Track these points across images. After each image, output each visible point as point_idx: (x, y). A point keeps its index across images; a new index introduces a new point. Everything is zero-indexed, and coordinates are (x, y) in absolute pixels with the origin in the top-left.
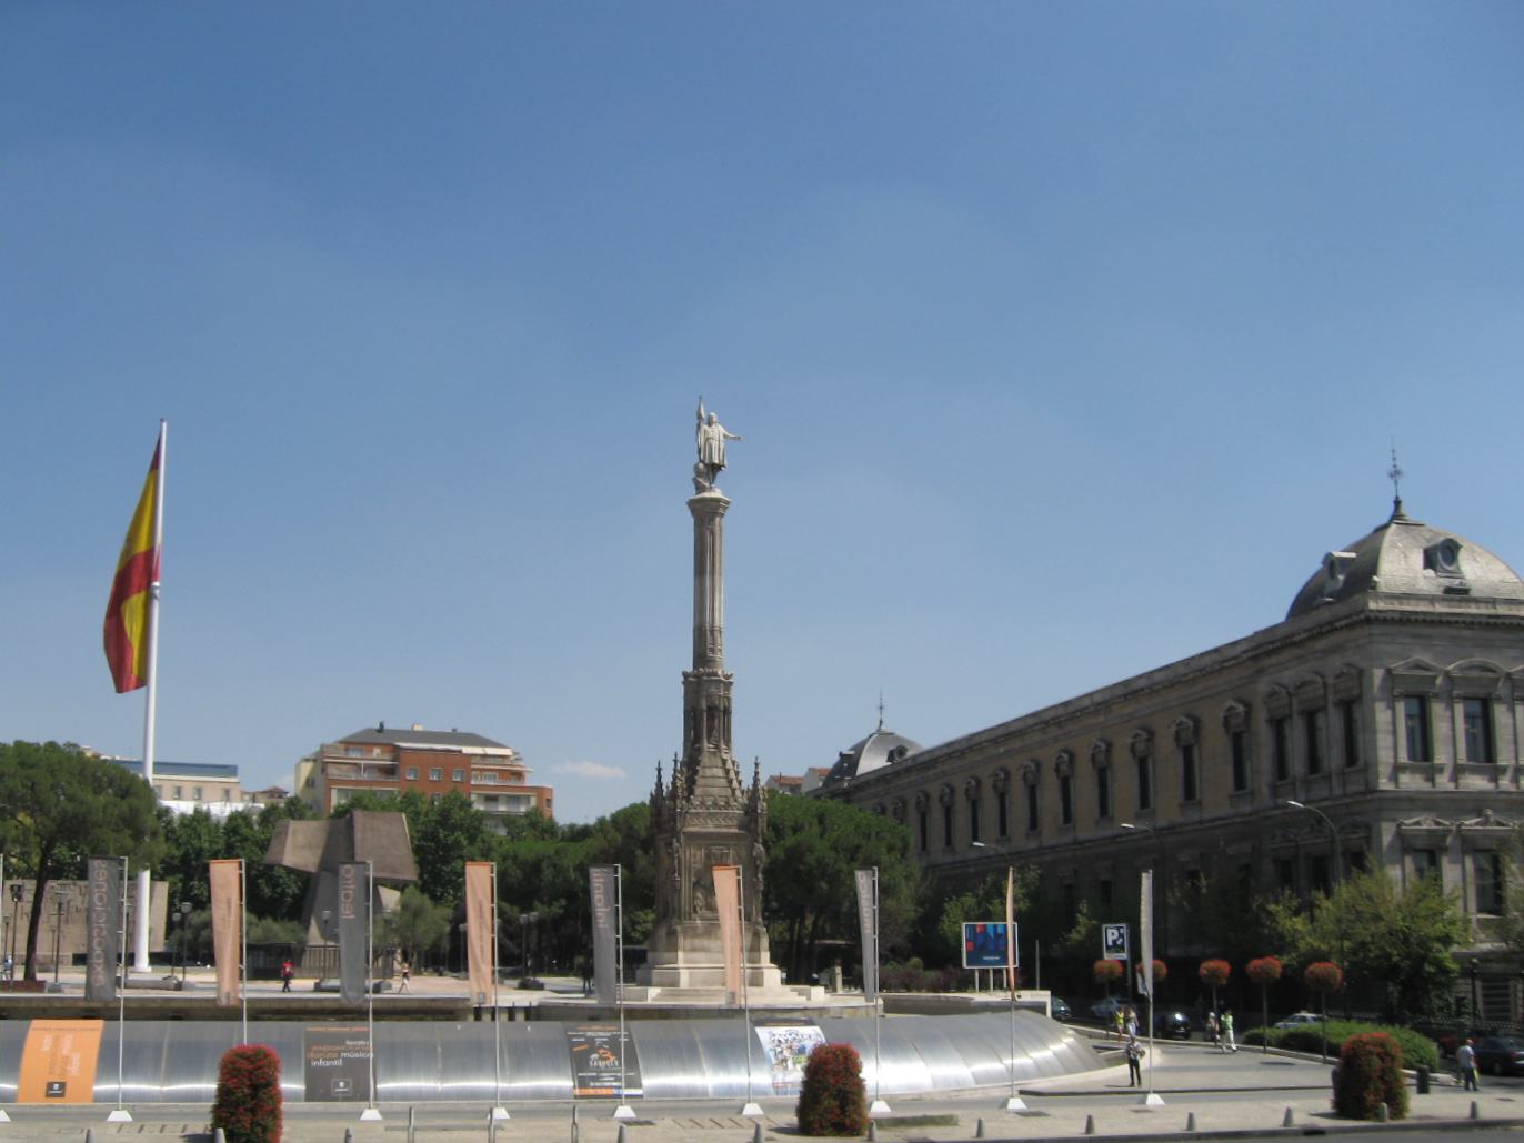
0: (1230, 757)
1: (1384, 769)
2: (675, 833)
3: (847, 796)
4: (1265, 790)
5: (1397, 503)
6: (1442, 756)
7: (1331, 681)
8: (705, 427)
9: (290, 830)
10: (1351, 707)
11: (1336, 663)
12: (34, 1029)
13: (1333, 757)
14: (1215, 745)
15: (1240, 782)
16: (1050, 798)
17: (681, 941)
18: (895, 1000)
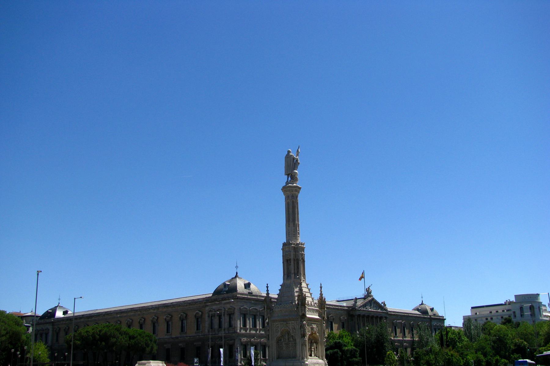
0: (196, 323)
1: (239, 328)
4: (206, 331)
5: (237, 273)
7: (227, 309)
10: (231, 315)
13: (225, 325)
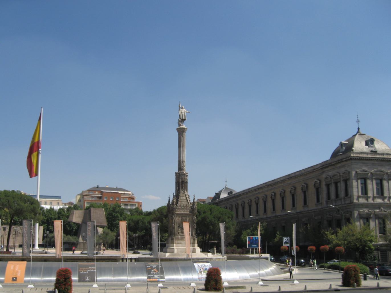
0: (316, 194)
1: (355, 197)
2: (173, 214)
3: (217, 204)
4: (325, 203)
5: (359, 129)
6: (370, 194)
7: (341, 174)
8: (181, 109)
9: (75, 213)
10: (347, 181)
11: (343, 170)
12: (9, 264)
13: (342, 194)
14: (312, 191)
15: (318, 200)
16: (269, 205)
17: (175, 241)
18: (230, 256)
